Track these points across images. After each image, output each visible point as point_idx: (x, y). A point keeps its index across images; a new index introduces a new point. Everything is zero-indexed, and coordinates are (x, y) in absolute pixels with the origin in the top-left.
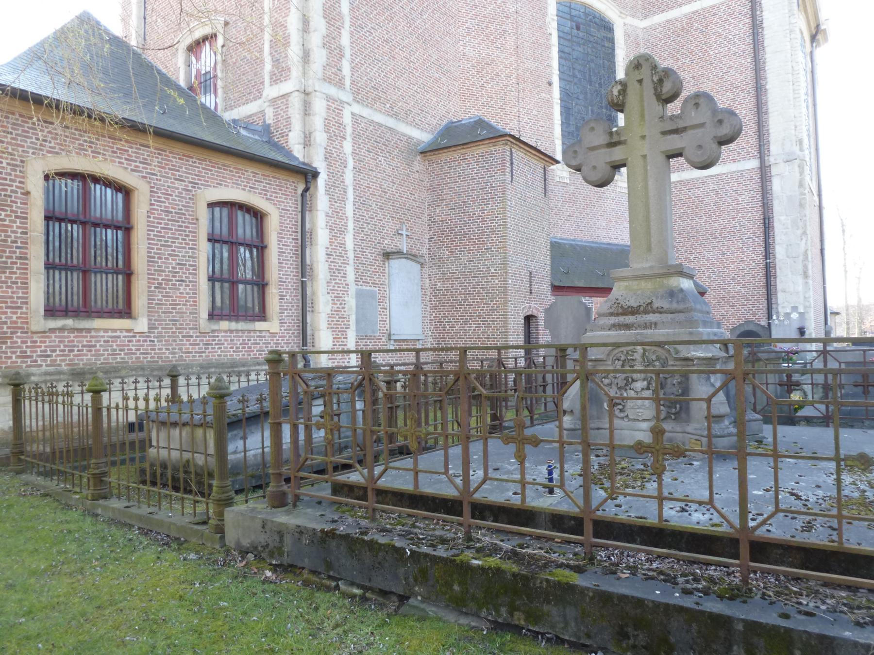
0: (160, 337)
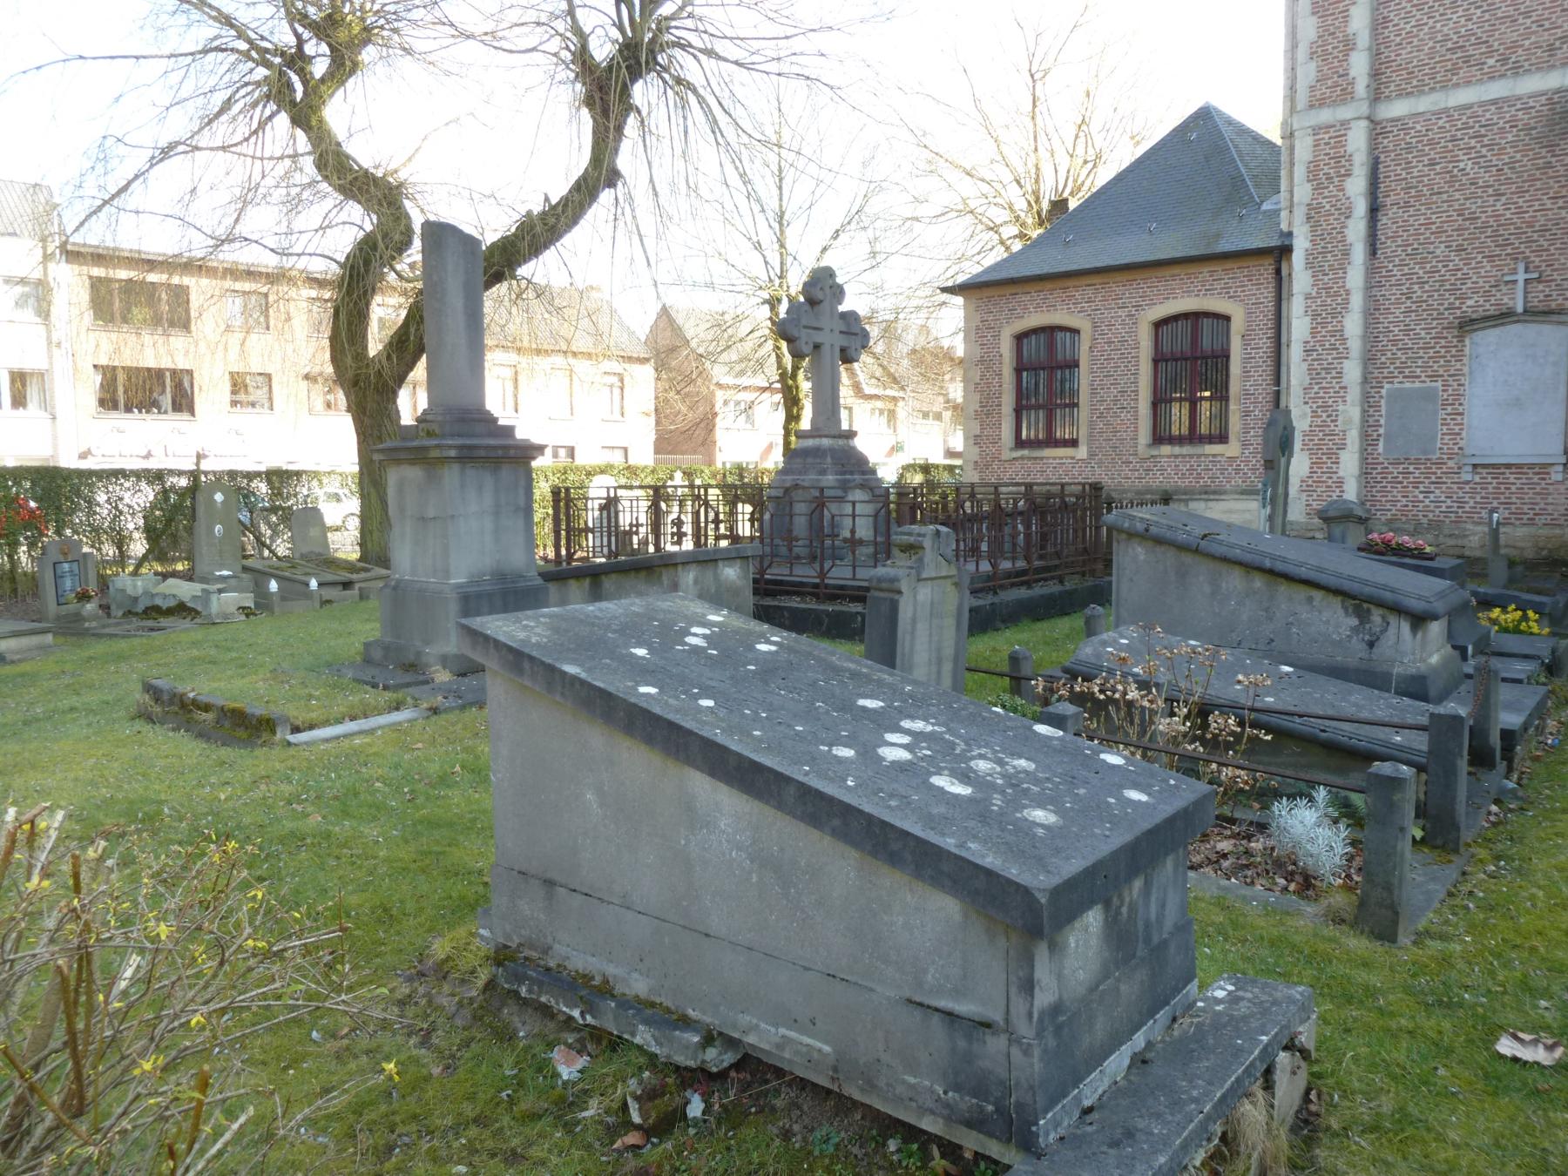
0: (1100, 463)
